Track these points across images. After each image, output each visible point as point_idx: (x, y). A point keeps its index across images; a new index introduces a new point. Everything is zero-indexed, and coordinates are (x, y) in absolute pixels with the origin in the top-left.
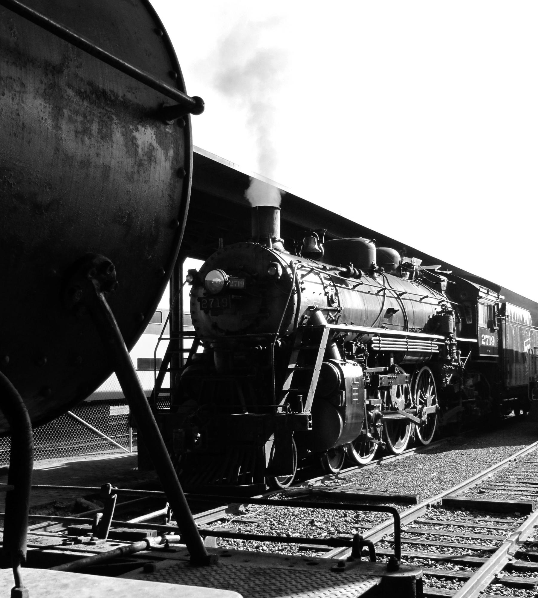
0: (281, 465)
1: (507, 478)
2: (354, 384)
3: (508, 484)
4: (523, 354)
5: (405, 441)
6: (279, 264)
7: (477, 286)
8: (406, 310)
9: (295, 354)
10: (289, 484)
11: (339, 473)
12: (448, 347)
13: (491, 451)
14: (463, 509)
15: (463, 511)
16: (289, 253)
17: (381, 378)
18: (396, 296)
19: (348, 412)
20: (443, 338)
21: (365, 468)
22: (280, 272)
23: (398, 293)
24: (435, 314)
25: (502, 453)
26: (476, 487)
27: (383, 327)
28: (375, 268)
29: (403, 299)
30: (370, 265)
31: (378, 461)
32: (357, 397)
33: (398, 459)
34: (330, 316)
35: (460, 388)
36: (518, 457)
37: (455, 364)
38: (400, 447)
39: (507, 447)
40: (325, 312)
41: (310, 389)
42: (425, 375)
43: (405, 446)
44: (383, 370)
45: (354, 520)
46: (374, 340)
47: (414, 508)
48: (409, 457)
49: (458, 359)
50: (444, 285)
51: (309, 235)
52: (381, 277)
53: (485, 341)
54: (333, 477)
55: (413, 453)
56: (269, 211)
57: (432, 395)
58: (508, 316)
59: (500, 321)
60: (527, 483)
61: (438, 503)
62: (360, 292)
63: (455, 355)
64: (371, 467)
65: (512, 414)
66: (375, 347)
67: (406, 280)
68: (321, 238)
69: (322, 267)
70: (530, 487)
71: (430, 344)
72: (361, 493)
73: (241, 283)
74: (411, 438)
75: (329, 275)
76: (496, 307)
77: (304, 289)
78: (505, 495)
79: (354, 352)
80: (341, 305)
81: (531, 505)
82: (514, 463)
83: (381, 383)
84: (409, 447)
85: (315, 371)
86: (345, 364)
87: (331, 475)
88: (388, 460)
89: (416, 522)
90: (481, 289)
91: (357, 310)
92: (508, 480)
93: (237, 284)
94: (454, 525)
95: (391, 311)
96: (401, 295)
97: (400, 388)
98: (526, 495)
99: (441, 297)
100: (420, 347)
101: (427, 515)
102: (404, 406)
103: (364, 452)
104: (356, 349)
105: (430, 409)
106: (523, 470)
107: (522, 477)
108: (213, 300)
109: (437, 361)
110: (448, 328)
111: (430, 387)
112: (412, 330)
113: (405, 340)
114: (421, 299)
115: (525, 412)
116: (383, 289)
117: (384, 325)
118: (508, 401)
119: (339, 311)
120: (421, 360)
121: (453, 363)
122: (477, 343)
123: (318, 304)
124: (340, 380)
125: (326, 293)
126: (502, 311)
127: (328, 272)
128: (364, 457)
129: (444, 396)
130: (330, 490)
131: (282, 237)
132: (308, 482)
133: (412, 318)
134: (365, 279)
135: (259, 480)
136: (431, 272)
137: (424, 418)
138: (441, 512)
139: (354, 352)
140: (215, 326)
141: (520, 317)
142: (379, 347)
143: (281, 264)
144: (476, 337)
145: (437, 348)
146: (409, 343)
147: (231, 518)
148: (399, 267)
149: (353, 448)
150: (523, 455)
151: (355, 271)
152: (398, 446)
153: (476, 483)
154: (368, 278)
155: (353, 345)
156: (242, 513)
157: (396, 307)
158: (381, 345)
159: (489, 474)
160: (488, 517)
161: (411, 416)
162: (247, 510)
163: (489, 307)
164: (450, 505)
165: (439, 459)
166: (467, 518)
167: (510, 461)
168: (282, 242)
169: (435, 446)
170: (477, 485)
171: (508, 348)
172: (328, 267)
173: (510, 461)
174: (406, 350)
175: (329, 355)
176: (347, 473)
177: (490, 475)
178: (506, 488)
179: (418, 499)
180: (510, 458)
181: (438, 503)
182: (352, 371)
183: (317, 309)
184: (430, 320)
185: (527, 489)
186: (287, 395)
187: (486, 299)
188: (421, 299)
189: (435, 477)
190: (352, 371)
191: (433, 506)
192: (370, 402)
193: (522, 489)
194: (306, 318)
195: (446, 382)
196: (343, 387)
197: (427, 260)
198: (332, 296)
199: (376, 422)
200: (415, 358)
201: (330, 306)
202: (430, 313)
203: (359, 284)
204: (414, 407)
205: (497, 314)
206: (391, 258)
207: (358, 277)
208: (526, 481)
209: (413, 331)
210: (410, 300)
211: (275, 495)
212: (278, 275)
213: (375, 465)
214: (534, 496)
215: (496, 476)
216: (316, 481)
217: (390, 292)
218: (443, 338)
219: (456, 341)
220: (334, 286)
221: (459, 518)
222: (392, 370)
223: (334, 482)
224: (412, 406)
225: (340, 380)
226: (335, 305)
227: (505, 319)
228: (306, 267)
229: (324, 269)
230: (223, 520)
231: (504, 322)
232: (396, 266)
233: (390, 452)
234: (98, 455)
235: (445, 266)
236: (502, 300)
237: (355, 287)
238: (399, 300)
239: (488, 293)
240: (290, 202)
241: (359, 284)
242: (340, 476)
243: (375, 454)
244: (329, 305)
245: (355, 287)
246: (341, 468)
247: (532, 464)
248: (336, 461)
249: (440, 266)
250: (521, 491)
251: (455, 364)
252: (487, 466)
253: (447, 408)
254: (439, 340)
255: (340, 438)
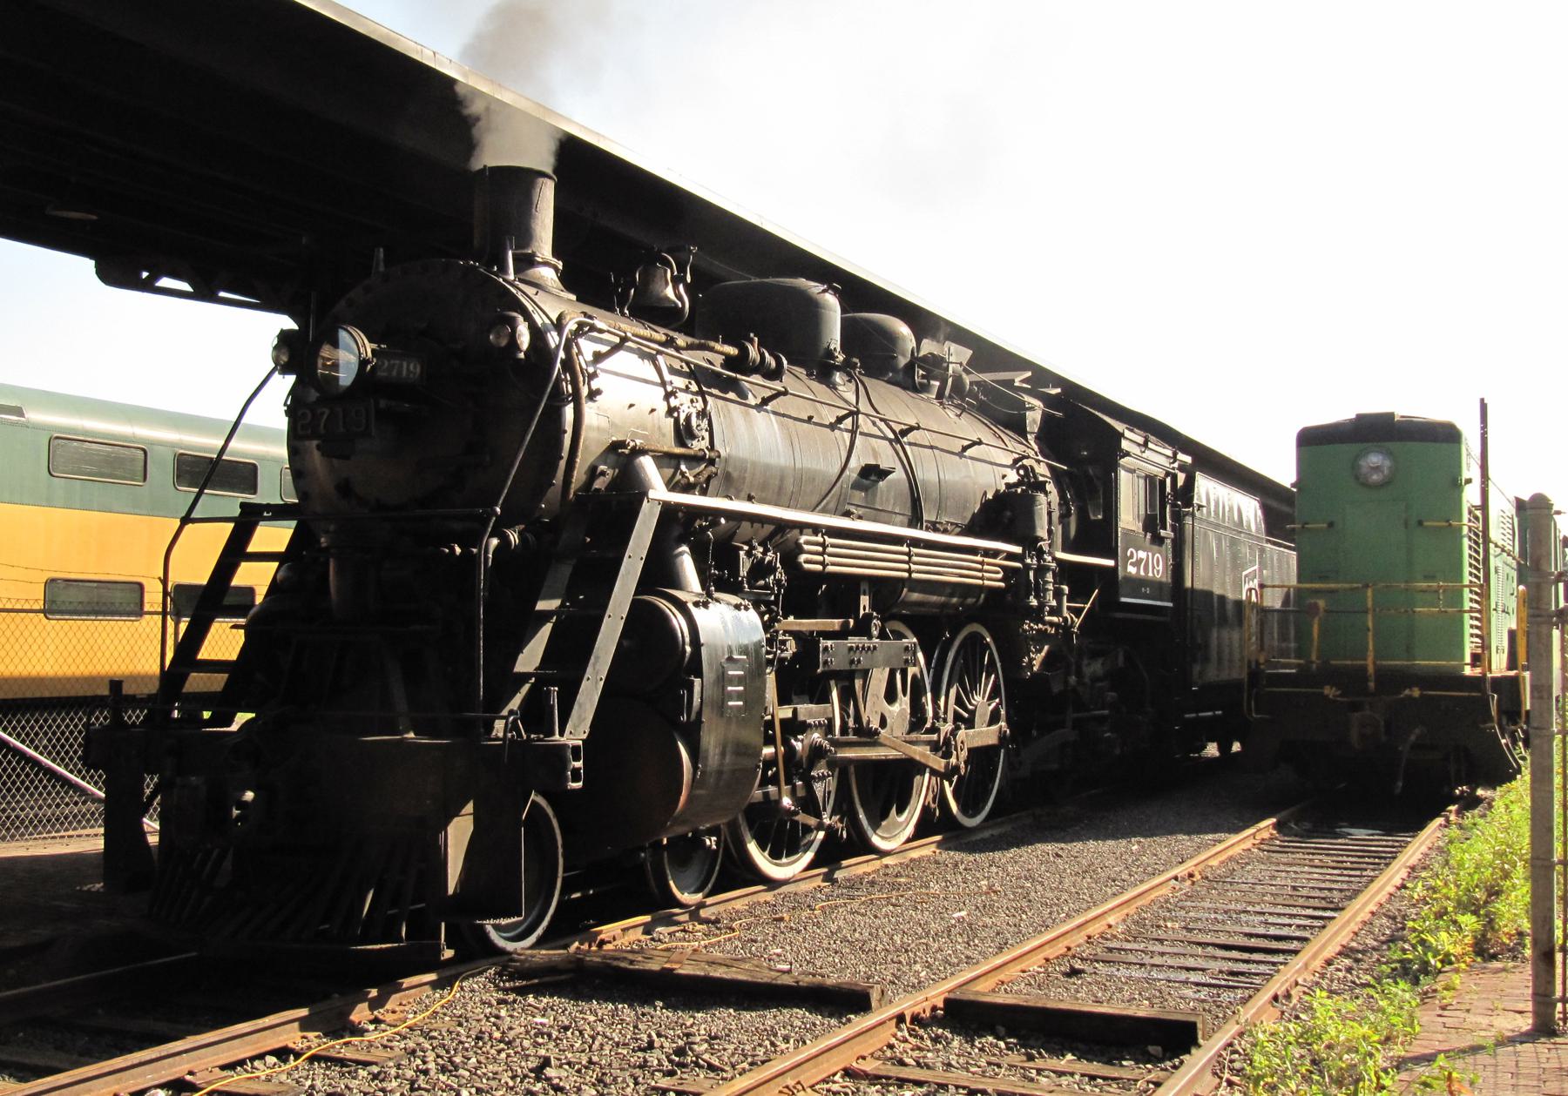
0: (492, 887)
1: (1159, 927)
2: (730, 659)
3: (1158, 948)
4: (1239, 604)
5: (908, 820)
6: (520, 319)
7: (1119, 426)
8: (919, 475)
9: (564, 572)
10: (532, 939)
11: (701, 905)
12: (1031, 574)
13: (1135, 847)
14: (1001, 1030)
15: (999, 1038)
16: (573, 297)
17: (826, 649)
18: (891, 436)
19: (711, 740)
20: (1018, 550)
21: (784, 889)
22: (524, 339)
23: (897, 428)
24: (1003, 488)
25: (1164, 852)
26: (1064, 956)
27: (847, 514)
28: (834, 358)
29: (910, 444)
30: (821, 352)
31: (825, 870)
32: (739, 696)
33: (887, 866)
34: (683, 474)
35: (1066, 682)
36: (1201, 867)
37: (1055, 619)
38: (894, 835)
39: (1180, 837)
40: (666, 461)
41: (589, 669)
42: (974, 646)
43: (910, 830)
44: (837, 628)
45: (670, 1061)
46: (808, 543)
47: (860, 1022)
48: (920, 859)
49: (1063, 611)
50: (1034, 418)
51: (652, 261)
52: (852, 386)
53: (1137, 564)
54: (685, 917)
55: (933, 848)
56: (519, 181)
57: (991, 698)
58: (1200, 507)
59: (1178, 518)
60: (1208, 944)
61: (934, 1009)
62: (784, 415)
63: (1050, 595)
64: (804, 887)
65: (1212, 750)
66: (807, 562)
67: (928, 400)
68: (681, 269)
69: (664, 338)
70: (1215, 958)
71: (983, 565)
72: (719, 973)
73: (410, 369)
74: (925, 809)
75: (688, 363)
76: (1168, 480)
77: (598, 392)
78: (1139, 980)
79: (743, 572)
80: (717, 446)
81: (1194, 1025)
82: (1188, 883)
83: (826, 663)
84: (922, 831)
85: (606, 619)
86: (706, 605)
87: (677, 910)
88: (855, 868)
89: (848, 1073)
90: (1128, 434)
91: (767, 467)
92: (1161, 934)
93: (400, 372)
94: (957, 1087)
95: (873, 473)
96: (904, 433)
97: (898, 676)
98: (1197, 984)
99: (1023, 448)
100: (951, 570)
101: (891, 1047)
102: (907, 726)
103: (783, 843)
104: (748, 565)
105: (985, 734)
106: (1207, 905)
107: (1200, 925)
108: (327, 412)
109: (1004, 607)
110: (1032, 526)
111: (988, 677)
112: (934, 527)
113: (905, 549)
114: (965, 449)
115: (243, 805)
116: (854, 414)
117: (847, 507)
118: (1198, 718)
119: (711, 462)
120: (955, 607)
121: (1047, 618)
122: (1114, 570)
123: (643, 437)
124: (688, 649)
125: (671, 411)
126: (1186, 494)
127: (686, 355)
128: (784, 860)
129: (1026, 703)
130: (632, 962)
131: (556, 253)
132: (600, 932)
133: (935, 495)
134: (795, 380)
135: (423, 931)
136: (994, 385)
137: (959, 758)
138: (936, 1040)
139: (743, 572)
140: (345, 489)
141: (1231, 509)
142: (823, 563)
143: (528, 317)
144: (1111, 552)
145: (1000, 576)
146: (915, 559)
147: (309, 1048)
148: (910, 367)
149: (748, 836)
150: (1214, 863)
151: (762, 356)
152: (888, 830)
153: (1066, 943)
154: (815, 385)
155: (742, 553)
156: (358, 1031)
157: (887, 459)
158: (828, 559)
159: (1111, 916)
160: (1069, 1057)
161: (921, 753)
162: (376, 1021)
163: (1150, 479)
164: (965, 1017)
165: (994, 869)
166: (1005, 1062)
167: (1176, 878)
168: (555, 268)
169: (996, 832)
170: (1069, 949)
171: (1199, 586)
172: (681, 340)
173: (1176, 878)
174: (906, 575)
175: (659, 574)
176: (729, 906)
177: (1111, 920)
178: (1147, 960)
179: (875, 996)
180: (1180, 871)
181: (934, 1009)
182: (725, 624)
183: (638, 452)
184: (987, 506)
185: (1201, 963)
186: (526, 687)
187: (1140, 462)
188: (965, 449)
189: (960, 921)
190: (725, 624)
191: (916, 1019)
192: (795, 711)
193: (1191, 962)
194: (603, 473)
195: (1030, 665)
196: (696, 667)
197: (987, 355)
198: (688, 418)
199: (811, 766)
200: (934, 598)
201: (684, 445)
202: (990, 486)
203: (779, 394)
204: (934, 730)
205: (1171, 505)
206: (891, 338)
207: (775, 374)
208: (1208, 938)
209: (936, 530)
210: (932, 447)
211: (481, 973)
212: (518, 348)
213: (818, 882)
214: (1220, 986)
215: (1129, 921)
216: (624, 930)
217: (874, 424)
218: (1018, 550)
219: (1054, 559)
220: (701, 393)
221: (983, 1063)
222: (863, 629)
223: (684, 931)
224: (928, 725)
225: (688, 649)
226: (698, 445)
227: (1193, 515)
228: (601, 331)
229: (670, 343)
230: (283, 1054)
231: (1188, 520)
232: (902, 361)
233: (863, 847)
234: (66, 840)
235: (1041, 376)
236: (1182, 468)
237: (765, 401)
238: (898, 447)
239: (1145, 445)
240: (580, 163)
241: (779, 394)
242: (703, 913)
243: (818, 853)
244: (680, 441)
245: (765, 401)
246: (707, 890)
247: (1236, 887)
248: (693, 873)
249: (1029, 374)
250: (1188, 969)
251: (1055, 619)
252: (1114, 889)
253: (1035, 733)
254: (1011, 556)
255: (683, 811)
